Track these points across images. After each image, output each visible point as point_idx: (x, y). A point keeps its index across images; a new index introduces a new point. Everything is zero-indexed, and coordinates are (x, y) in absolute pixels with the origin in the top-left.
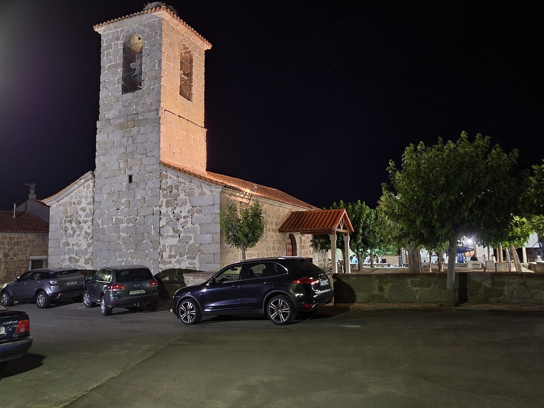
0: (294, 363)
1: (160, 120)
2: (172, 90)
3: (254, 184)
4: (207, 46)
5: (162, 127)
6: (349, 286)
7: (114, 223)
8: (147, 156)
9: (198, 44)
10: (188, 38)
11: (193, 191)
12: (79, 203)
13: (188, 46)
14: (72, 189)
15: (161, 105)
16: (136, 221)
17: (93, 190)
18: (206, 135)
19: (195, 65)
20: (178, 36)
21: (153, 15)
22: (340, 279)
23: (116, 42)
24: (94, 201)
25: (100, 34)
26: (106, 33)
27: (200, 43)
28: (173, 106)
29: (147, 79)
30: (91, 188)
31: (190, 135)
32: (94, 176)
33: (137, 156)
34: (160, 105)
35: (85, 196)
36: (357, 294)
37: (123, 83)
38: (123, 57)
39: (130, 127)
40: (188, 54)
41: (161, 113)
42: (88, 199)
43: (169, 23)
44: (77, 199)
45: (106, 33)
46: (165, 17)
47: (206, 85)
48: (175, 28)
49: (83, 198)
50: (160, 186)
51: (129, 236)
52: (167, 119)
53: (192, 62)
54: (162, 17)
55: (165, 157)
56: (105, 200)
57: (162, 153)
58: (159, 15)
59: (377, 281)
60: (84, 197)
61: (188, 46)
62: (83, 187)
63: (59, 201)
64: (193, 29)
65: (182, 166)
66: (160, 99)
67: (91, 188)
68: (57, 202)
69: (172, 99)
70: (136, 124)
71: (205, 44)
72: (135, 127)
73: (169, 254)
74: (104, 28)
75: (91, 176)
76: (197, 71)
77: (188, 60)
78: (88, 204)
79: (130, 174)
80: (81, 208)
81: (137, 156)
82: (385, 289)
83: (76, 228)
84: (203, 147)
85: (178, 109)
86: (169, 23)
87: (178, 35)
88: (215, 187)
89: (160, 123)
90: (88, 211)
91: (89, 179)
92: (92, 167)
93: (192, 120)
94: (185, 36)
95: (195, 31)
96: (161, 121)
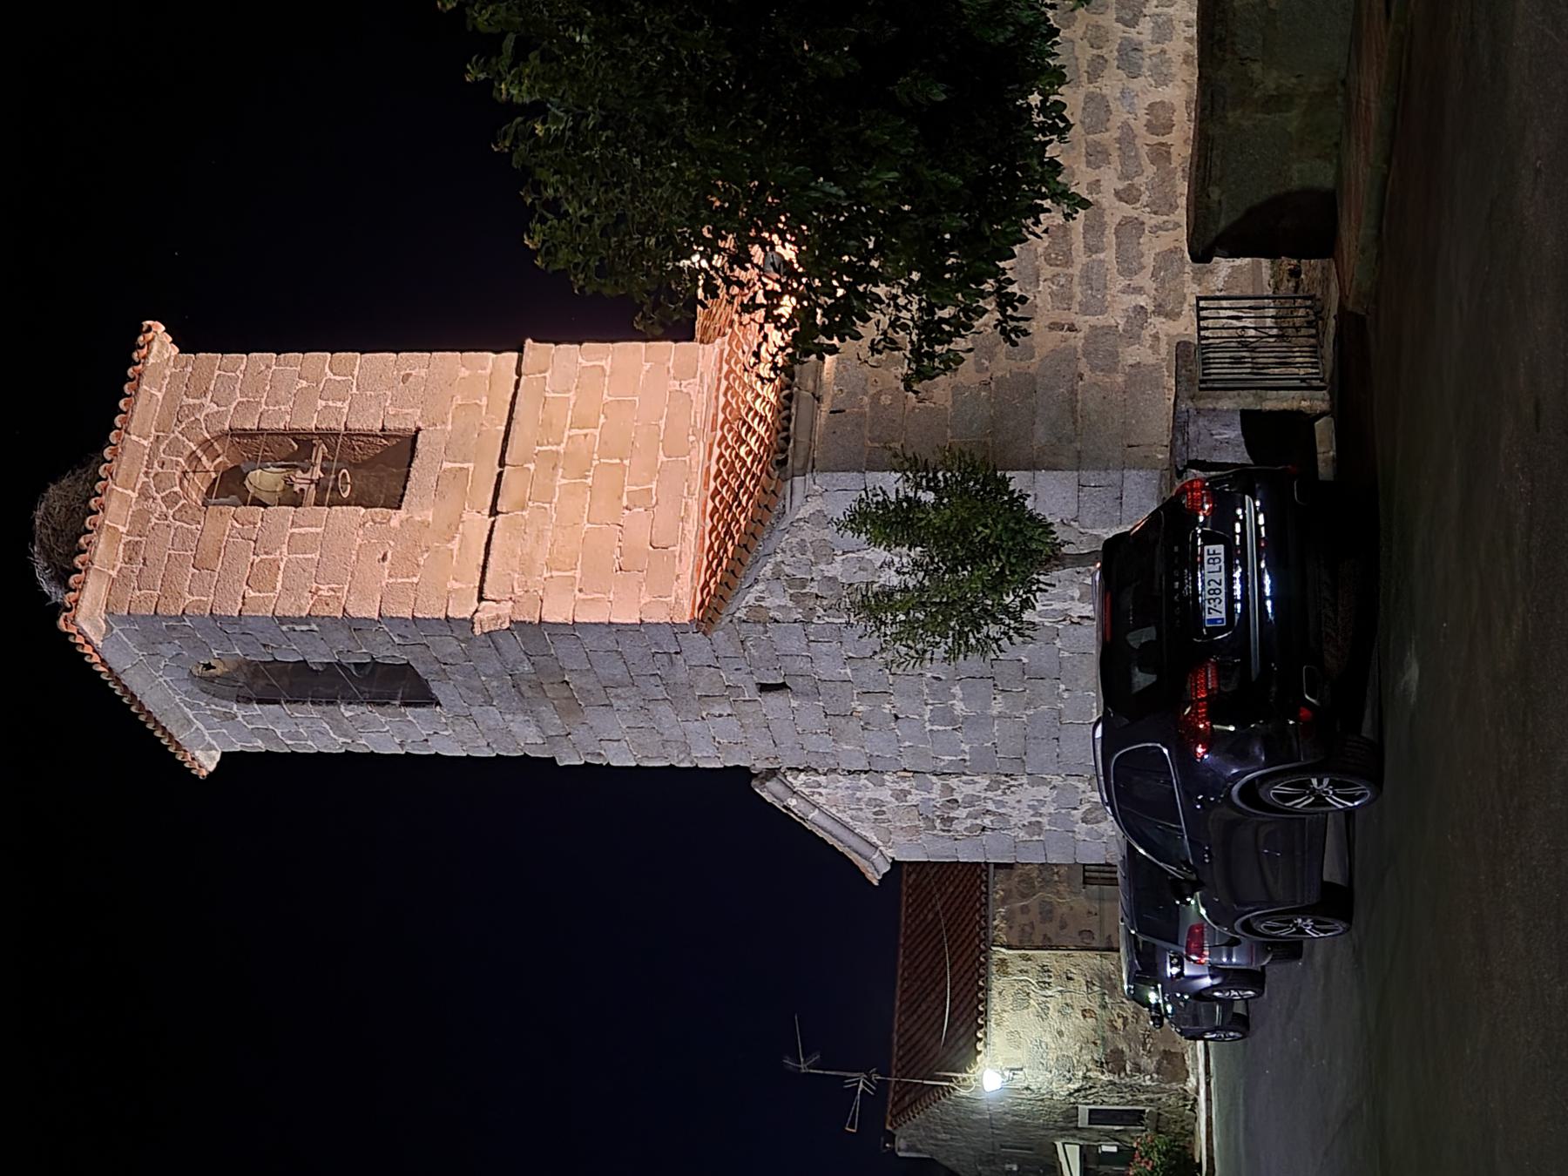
1: (525, 622)
2: (389, 555)
4: (155, 346)
5: (556, 613)
6: (1250, 212)
7: (950, 728)
8: (676, 653)
9: (160, 395)
10: (149, 465)
11: (811, 543)
13: (181, 460)
14: (828, 824)
15: (461, 616)
16: (943, 678)
17: (825, 774)
18: (552, 345)
19: (253, 416)
20: (154, 520)
21: (106, 642)
22: (1218, 238)
23: (240, 719)
24: (866, 772)
25: (223, 754)
26: (214, 743)
27: (154, 391)
28: (455, 545)
29: (364, 650)
30: (818, 779)
31: (561, 448)
32: (772, 773)
33: (681, 676)
34: (464, 619)
36: (1296, 184)
37: (397, 703)
38: (295, 702)
39: (567, 694)
40: (215, 444)
41: (496, 625)
43: (114, 574)
44: (864, 806)
45: (214, 743)
46: (98, 604)
47: (333, 346)
48: (126, 539)
50: (796, 625)
51: (1004, 694)
52: (516, 585)
53: (245, 430)
54: (103, 615)
55: (674, 595)
56: (863, 747)
57: (660, 616)
58: (99, 628)
59: (1232, 116)
61: (181, 460)
63: (871, 844)
64: (107, 453)
65: (702, 498)
66: (439, 619)
67: (818, 779)
68: (877, 848)
69: (426, 555)
70: (561, 679)
71: (151, 360)
72: (566, 679)
73: (1077, 602)
74: (198, 753)
75: (773, 785)
76: (277, 403)
77: (239, 443)
79: (755, 689)
81: (681, 676)
82: (1277, 88)
83: (971, 809)
84: (603, 363)
85: (465, 517)
86: (114, 574)
87: (149, 521)
88: (788, 500)
89: (537, 622)
91: (786, 785)
92: (742, 775)
93: (499, 431)
94: (143, 478)
95: (112, 437)
96: (527, 619)
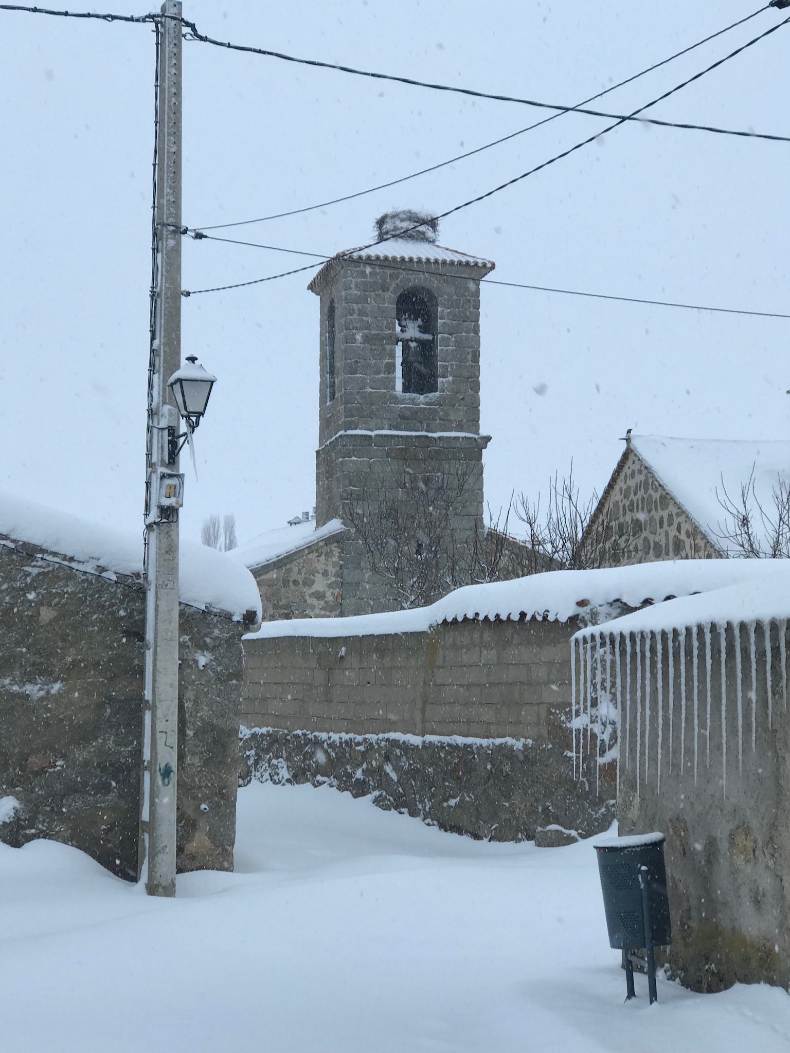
0: (411, 762)
3: (646, 959)
12: (309, 583)
23: (380, 292)
35: (321, 572)
42: (329, 577)
49: (317, 575)
60: (319, 573)
62: (317, 554)
78: (330, 586)
80: (312, 593)
90: (329, 598)
